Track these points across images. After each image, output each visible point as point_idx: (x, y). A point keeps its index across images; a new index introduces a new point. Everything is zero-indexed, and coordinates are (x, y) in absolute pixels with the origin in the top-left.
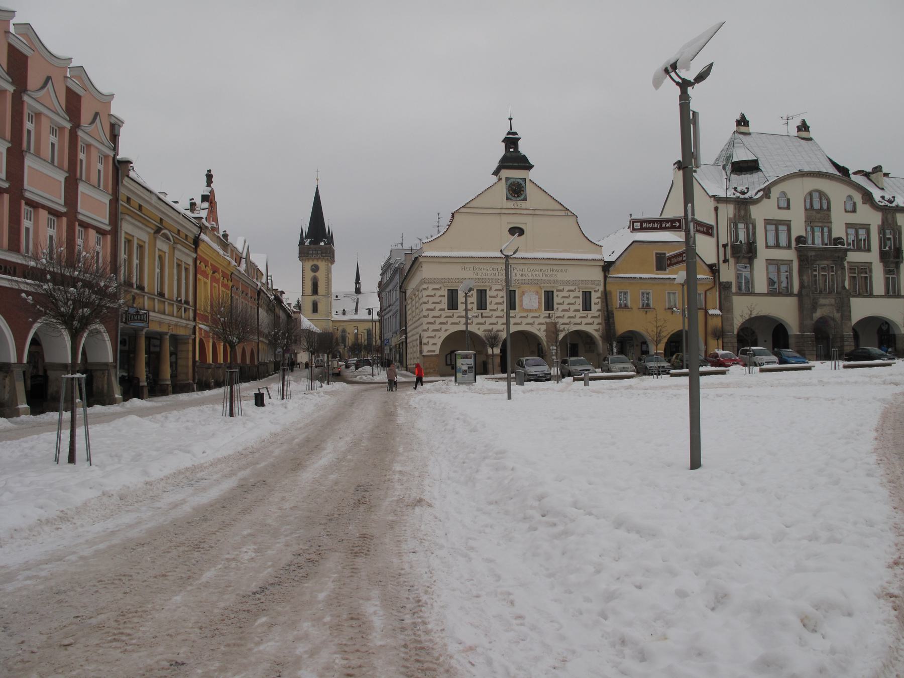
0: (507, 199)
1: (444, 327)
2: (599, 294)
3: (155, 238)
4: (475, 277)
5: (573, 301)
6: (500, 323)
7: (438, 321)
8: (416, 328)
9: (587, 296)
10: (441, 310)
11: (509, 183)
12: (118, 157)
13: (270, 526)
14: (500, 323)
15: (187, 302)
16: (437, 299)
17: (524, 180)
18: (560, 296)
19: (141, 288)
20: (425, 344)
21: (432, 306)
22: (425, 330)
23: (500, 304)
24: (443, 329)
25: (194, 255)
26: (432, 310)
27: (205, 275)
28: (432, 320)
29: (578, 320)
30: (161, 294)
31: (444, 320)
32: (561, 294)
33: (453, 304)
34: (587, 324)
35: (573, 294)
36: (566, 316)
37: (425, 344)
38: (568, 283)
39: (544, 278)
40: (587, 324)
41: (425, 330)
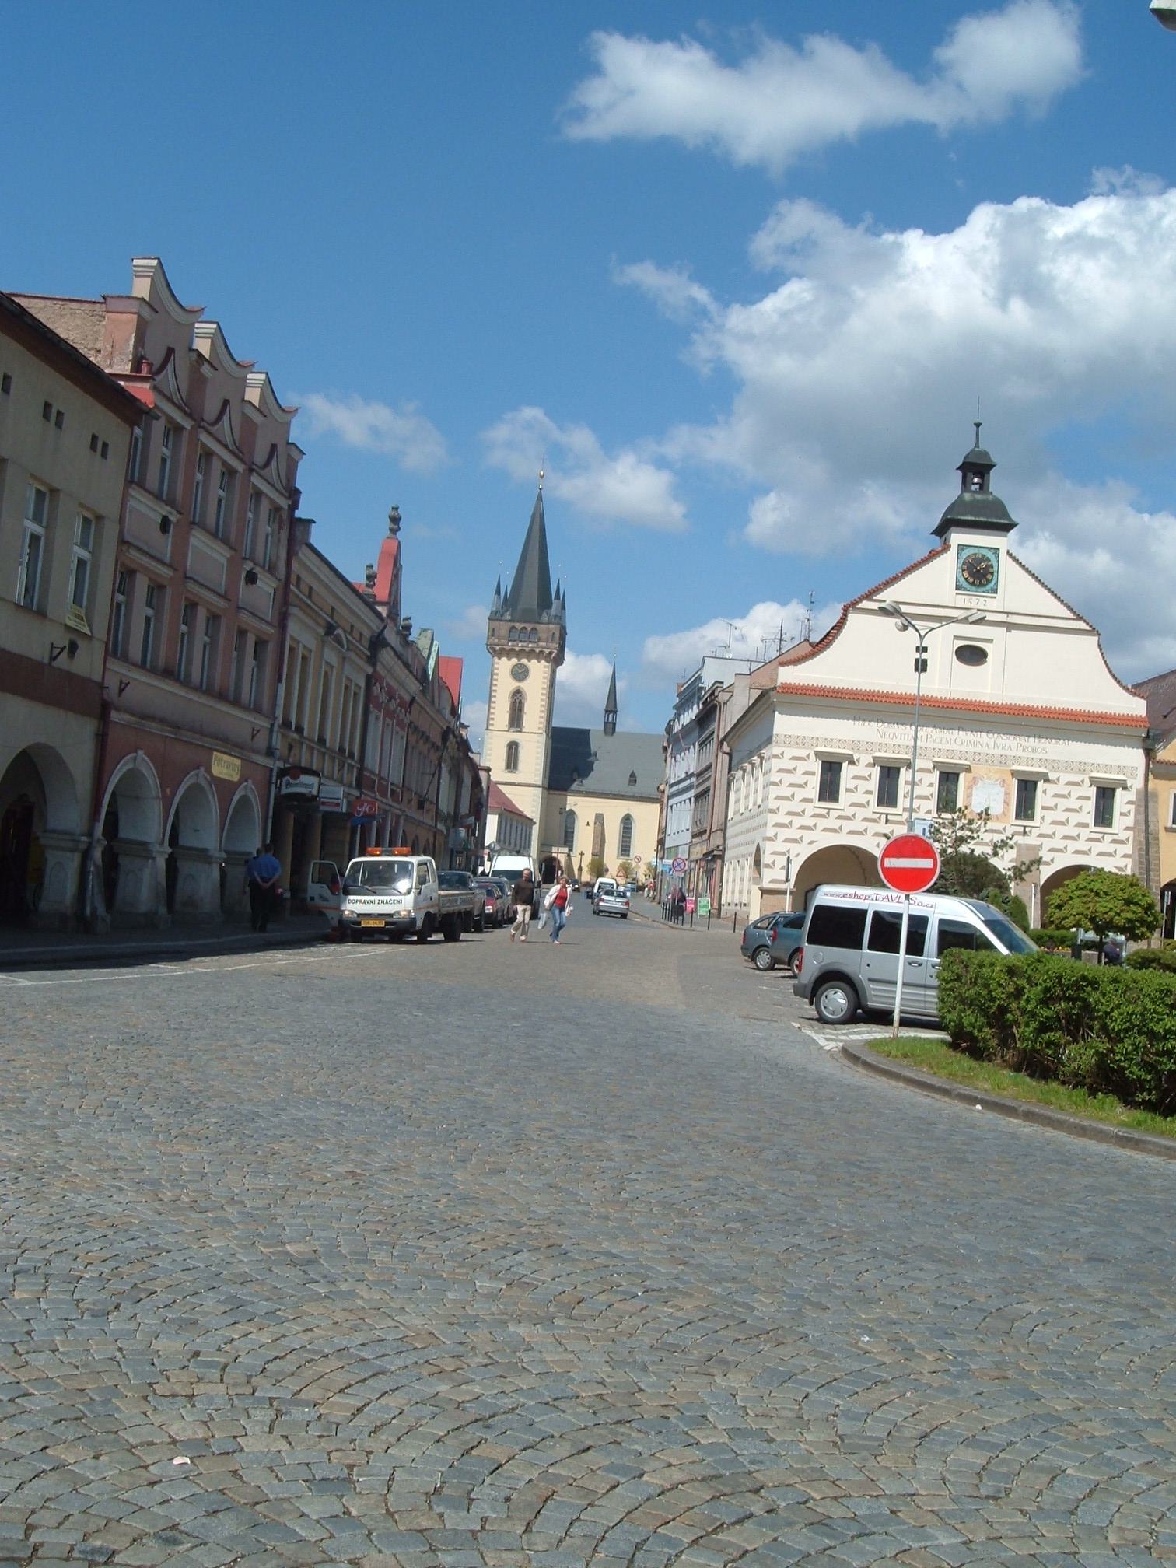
0: (958, 588)
1: (808, 836)
2: (1131, 796)
3: (323, 642)
4: (880, 740)
5: (1076, 805)
6: (1120, 853)
7: (797, 821)
8: (750, 831)
9: (1105, 794)
10: (805, 800)
11: (964, 555)
12: (298, 514)
13: (504, 1125)
14: (1120, 853)
15: (351, 755)
16: (799, 778)
17: (996, 551)
18: (1050, 793)
19: (299, 730)
20: (767, 866)
21: (788, 792)
22: (770, 839)
23: (926, 798)
24: (806, 840)
25: (370, 670)
26: (789, 771)
27: (378, 707)
28: (786, 820)
29: (1083, 845)
30: (322, 741)
31: (810, 822)
32: (1051, 789)
33: (829, 790)
34: (1101, 854)
35: (1077, 792)
36: (1059, 835)
37: (767, 866)
38: (1068, 767)
39: (1020, 753)
40: (1101, 854)
41: (770, 839)
